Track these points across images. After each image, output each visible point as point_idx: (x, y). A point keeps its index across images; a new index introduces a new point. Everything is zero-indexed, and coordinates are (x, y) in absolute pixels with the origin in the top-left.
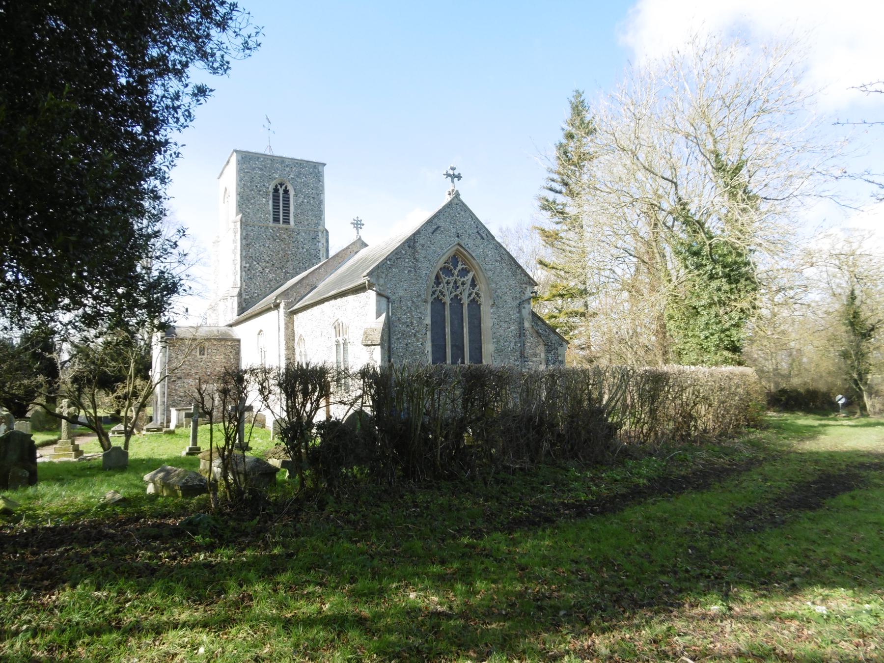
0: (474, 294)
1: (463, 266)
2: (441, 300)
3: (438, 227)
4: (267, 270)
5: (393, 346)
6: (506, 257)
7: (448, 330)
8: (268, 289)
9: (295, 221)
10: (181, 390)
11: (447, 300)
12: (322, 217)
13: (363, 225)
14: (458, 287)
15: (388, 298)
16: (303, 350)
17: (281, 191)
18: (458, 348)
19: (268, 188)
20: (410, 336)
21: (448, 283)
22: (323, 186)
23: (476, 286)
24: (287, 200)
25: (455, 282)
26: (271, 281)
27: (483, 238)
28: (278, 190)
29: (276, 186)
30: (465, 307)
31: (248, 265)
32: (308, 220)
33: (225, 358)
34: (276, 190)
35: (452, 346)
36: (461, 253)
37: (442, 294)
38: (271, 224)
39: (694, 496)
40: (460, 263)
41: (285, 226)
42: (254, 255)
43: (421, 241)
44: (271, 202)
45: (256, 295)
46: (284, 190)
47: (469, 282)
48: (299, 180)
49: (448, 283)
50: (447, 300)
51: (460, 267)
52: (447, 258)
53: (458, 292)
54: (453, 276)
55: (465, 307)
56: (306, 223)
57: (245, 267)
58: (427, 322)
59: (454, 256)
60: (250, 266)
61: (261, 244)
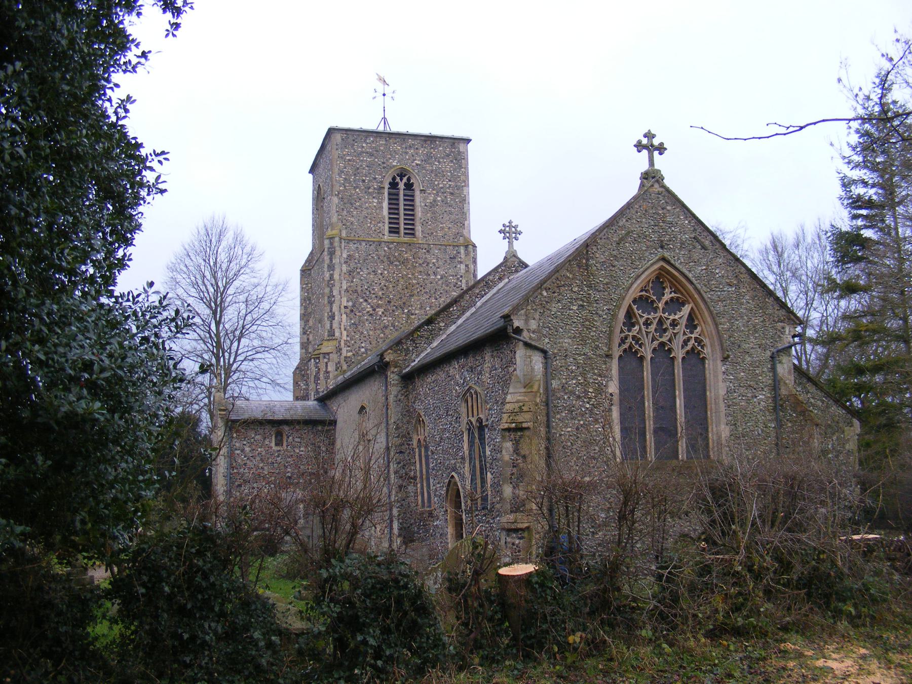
0: (630, 340)
1: (673, 295)
2: (636, 352)
3: (628, 233)
4: (380, 311)
6: (745, 277)
7: (648, 404)
8: (381, 341)
11: (647, 352)
12: (466, 223)
13: (500, 232)
14: (665, 330)
15: (544, 352)
16: (422, 438)
17: (401, 186)
18: (666, 431)
19: (382, 182)
21: (647, 323)
22: (466, 175)
23: (695, 327)
24: (410, 199)
25: (661, 322)
26: (386, 327)
27: (704, 247)
28: (397, 184)
29: (394, 178)
30: (678, 363)
31: (350, 304)
34: (394, 185)
35: (656, 431)
36: (668, 273)
37: (637, 343)
39: (228, 650)
40: (667, 290)
41: (406, 239)
42: (359, 289)
43: (600, 257)
44: (385, 205)
45: (363, 350)
46: (405, 184)
47: (684, 322)
48: (428, 167)
49: (647, 323)
50: (647, 352)
51: (667, 296)
52: (643, 284)
53: (664, 339)
54: (655, 312)
55: (678, 363)
58: (610, 390)
59: (658, 278)
60: (354, 306)
61: (371, 270)
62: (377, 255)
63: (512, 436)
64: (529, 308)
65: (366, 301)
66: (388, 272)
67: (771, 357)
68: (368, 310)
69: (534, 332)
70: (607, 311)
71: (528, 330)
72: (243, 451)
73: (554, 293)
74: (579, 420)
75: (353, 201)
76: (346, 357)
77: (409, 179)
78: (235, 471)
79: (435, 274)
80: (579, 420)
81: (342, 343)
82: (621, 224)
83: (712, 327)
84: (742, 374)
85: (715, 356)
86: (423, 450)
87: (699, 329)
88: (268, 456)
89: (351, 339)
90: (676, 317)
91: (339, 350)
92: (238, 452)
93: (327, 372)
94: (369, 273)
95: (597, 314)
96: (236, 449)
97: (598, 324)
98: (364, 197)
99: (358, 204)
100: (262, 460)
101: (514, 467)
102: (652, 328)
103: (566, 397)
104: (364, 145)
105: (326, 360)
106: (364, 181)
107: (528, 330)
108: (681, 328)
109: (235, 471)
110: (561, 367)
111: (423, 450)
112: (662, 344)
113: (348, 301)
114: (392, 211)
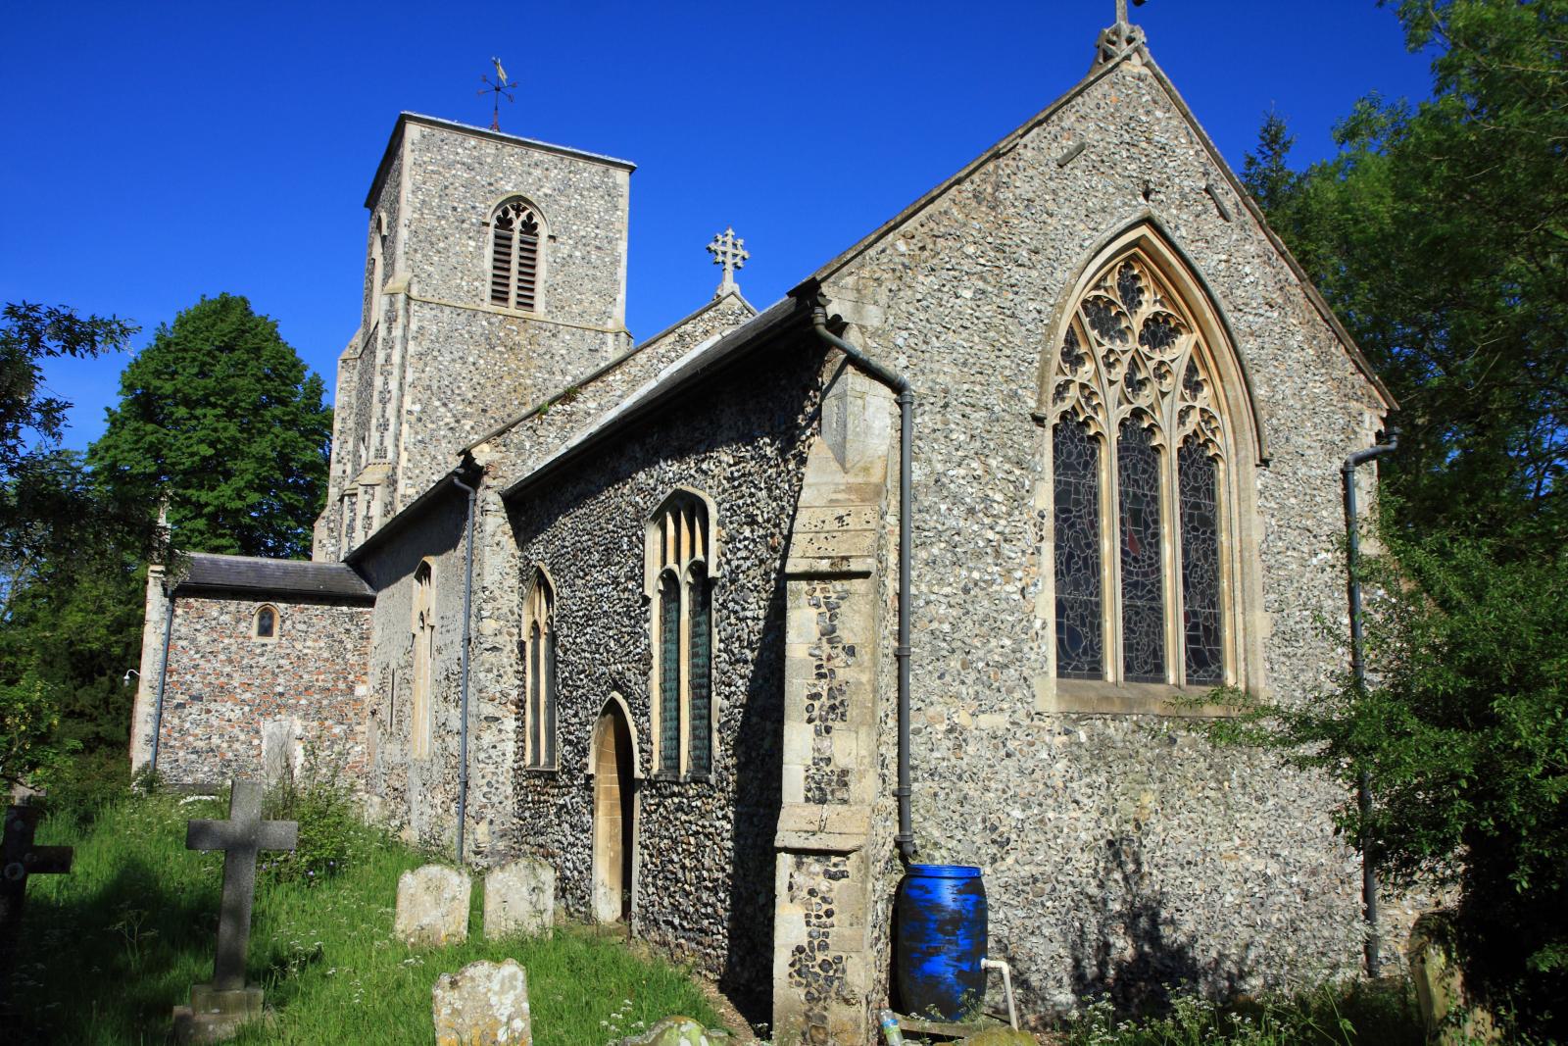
0: (1074, 392)
1: (1158, 308)
3: (1080, 148)
4: (468, 424)
5: (913, 590)
9: (548, 303)
10: (198, 731)
11: (1108, 423)
14: (1142, 383)
15: (897, 387)
17: (517, 225)
20: (979, 555)
24: (529, 249)
27: (1224, 215)
28: (510, 222)
31: (417, 408)
32: (580, 302)
33: (331, 647)
34: (504, 223)
38: (487, 305)
40: (1146, 297)
41: (520, 313)
44: (489, 251)
46: (524, 224)
47: (1180, 369)
48: (563, 201)
51: (1149, 306)
53: (1142, 402)
56: (576, 309)
57: (410, 412)
60: (423, 411)
61: (456, 355)
62: (469, 332)
63: (818, 594)
64: (865, 272)
65: (445, 405)
66: (486, 363)
67: (1342, 471)
68: (447, 420)
69: (873, 335)
70: (1035, 314)
71: (862, 328)
72: (193, 641)
73: (923, 248)
74: (970, 570)
75: (434, 239)
76: (404, 496)
77: (530, 216)
78: (175, 678)
79: (563, 373)
80: (970, 570)
81: (400, 472)
82: (1066, 124)
83: (1238, 390)
84: (1293, 500)
85: (1242, 454)
86: (543, 643)
87: (1207, 391)
88: (242, 653)
89: (416, 466)
90: (1166, 358)
91: (392, 482)
92: (184, 643)
93: (368, 518)
94: (454, 360)
95: (1013, 316)
96: (180, 638)
97: (1017, 341)
98: (453, 235)
99: (442, 245)
100: (230, 661)
101: (821, 676)
102: (1120, 372)
103: (943, 507)
104: (460, 150)
105: (367, 497)
106: (455, 209)
107: (862, 328)
108: (1174, 383)
109: (175, 678)
110: (934, 431)
111: (543, 643)
112: (1138, 413)
113: (413, 403)
114: (499, 264)
